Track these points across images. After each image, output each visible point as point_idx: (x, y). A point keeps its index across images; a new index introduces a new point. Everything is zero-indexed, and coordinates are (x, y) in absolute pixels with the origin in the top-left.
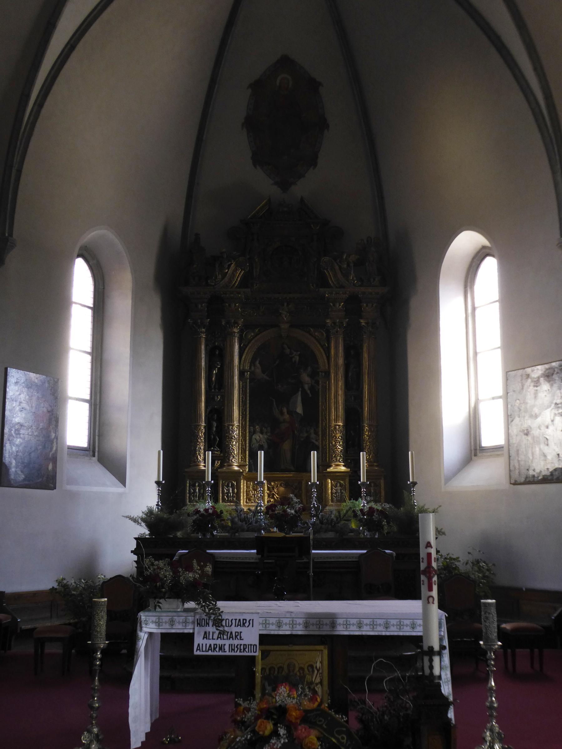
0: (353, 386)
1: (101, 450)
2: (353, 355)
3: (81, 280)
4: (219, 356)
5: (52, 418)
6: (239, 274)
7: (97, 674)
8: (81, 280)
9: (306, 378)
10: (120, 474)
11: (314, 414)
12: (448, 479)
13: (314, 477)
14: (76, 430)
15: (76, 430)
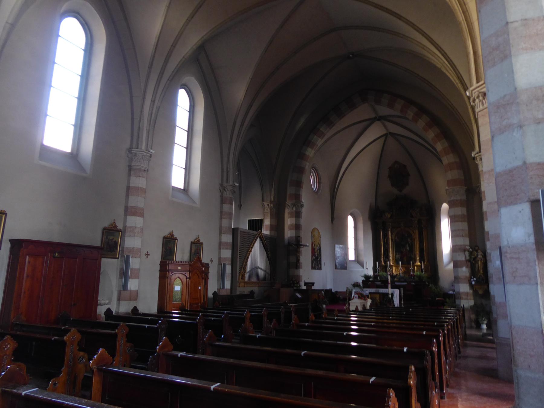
0: (421, 242)
1: (358, 260)
2: (421, 234)
3: (350, 221)
4: (386, 236)
5: (346, 254)
6: (389, 216)
7: (348, 356)
8: (350, 221)
9: (409, 240)
10: (362, 266)
11: (412, 250)
12: (445, 267)
13: (412, 267)
14: (352, 256)
15: (352, 256)
